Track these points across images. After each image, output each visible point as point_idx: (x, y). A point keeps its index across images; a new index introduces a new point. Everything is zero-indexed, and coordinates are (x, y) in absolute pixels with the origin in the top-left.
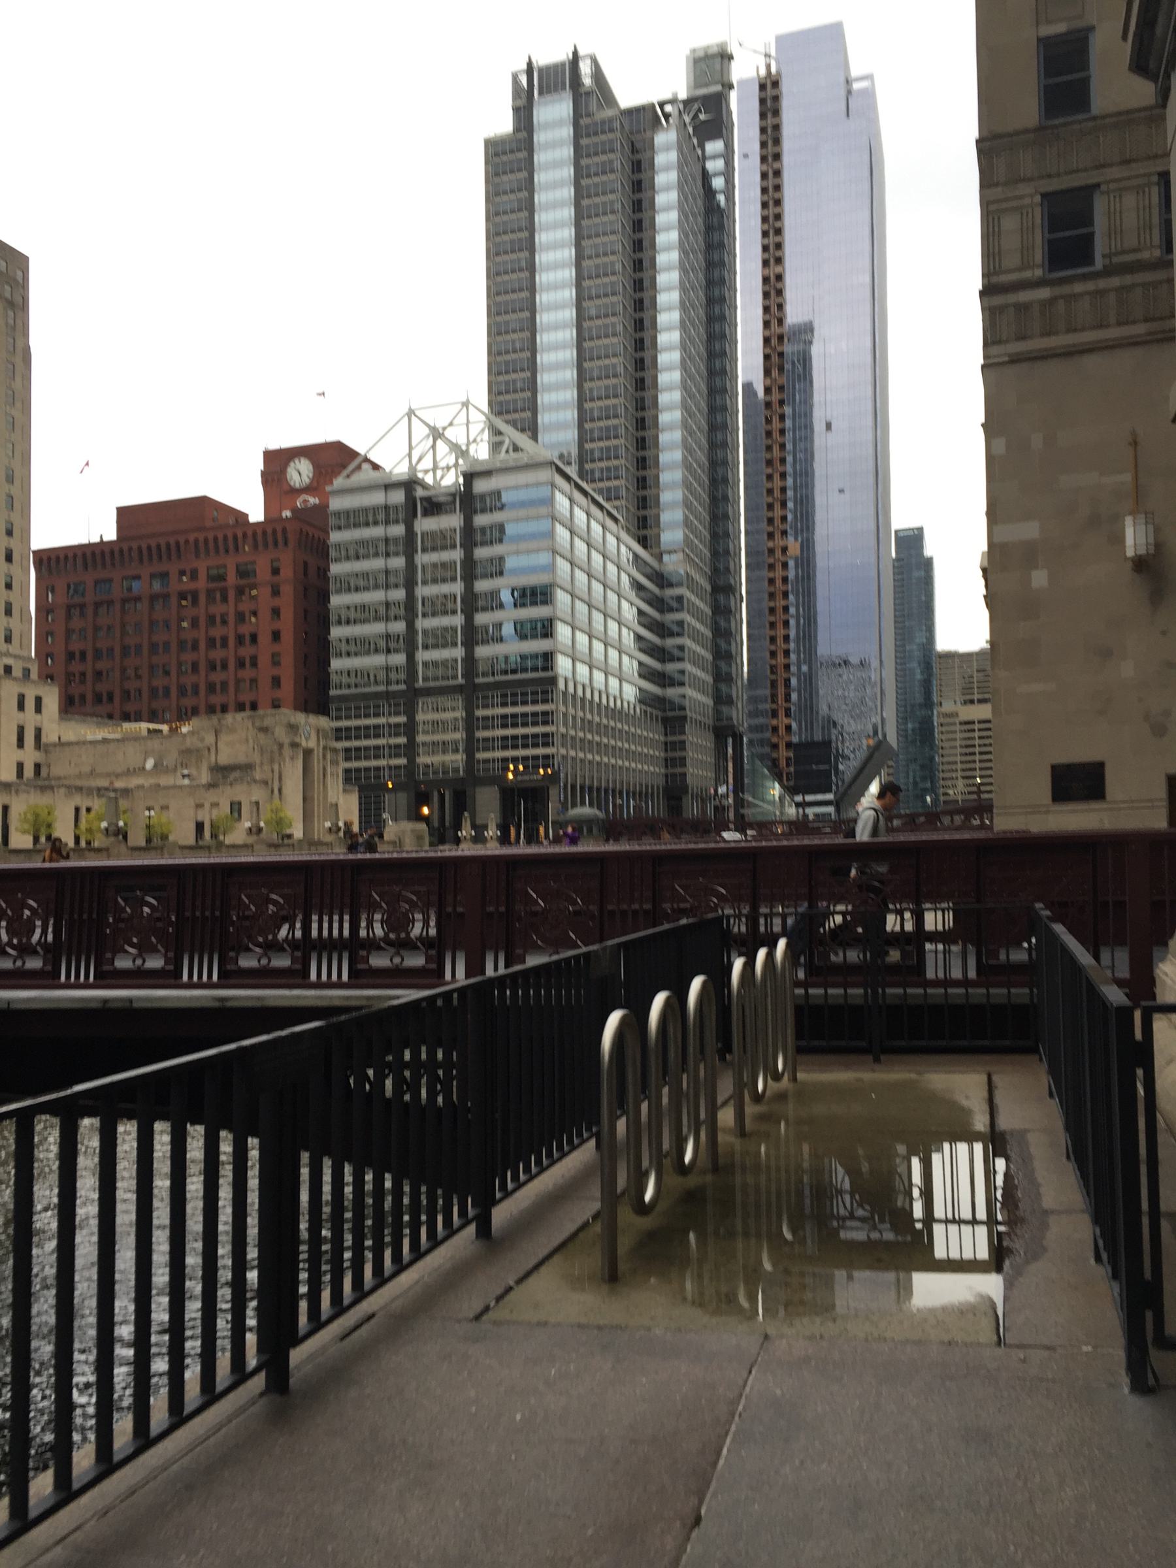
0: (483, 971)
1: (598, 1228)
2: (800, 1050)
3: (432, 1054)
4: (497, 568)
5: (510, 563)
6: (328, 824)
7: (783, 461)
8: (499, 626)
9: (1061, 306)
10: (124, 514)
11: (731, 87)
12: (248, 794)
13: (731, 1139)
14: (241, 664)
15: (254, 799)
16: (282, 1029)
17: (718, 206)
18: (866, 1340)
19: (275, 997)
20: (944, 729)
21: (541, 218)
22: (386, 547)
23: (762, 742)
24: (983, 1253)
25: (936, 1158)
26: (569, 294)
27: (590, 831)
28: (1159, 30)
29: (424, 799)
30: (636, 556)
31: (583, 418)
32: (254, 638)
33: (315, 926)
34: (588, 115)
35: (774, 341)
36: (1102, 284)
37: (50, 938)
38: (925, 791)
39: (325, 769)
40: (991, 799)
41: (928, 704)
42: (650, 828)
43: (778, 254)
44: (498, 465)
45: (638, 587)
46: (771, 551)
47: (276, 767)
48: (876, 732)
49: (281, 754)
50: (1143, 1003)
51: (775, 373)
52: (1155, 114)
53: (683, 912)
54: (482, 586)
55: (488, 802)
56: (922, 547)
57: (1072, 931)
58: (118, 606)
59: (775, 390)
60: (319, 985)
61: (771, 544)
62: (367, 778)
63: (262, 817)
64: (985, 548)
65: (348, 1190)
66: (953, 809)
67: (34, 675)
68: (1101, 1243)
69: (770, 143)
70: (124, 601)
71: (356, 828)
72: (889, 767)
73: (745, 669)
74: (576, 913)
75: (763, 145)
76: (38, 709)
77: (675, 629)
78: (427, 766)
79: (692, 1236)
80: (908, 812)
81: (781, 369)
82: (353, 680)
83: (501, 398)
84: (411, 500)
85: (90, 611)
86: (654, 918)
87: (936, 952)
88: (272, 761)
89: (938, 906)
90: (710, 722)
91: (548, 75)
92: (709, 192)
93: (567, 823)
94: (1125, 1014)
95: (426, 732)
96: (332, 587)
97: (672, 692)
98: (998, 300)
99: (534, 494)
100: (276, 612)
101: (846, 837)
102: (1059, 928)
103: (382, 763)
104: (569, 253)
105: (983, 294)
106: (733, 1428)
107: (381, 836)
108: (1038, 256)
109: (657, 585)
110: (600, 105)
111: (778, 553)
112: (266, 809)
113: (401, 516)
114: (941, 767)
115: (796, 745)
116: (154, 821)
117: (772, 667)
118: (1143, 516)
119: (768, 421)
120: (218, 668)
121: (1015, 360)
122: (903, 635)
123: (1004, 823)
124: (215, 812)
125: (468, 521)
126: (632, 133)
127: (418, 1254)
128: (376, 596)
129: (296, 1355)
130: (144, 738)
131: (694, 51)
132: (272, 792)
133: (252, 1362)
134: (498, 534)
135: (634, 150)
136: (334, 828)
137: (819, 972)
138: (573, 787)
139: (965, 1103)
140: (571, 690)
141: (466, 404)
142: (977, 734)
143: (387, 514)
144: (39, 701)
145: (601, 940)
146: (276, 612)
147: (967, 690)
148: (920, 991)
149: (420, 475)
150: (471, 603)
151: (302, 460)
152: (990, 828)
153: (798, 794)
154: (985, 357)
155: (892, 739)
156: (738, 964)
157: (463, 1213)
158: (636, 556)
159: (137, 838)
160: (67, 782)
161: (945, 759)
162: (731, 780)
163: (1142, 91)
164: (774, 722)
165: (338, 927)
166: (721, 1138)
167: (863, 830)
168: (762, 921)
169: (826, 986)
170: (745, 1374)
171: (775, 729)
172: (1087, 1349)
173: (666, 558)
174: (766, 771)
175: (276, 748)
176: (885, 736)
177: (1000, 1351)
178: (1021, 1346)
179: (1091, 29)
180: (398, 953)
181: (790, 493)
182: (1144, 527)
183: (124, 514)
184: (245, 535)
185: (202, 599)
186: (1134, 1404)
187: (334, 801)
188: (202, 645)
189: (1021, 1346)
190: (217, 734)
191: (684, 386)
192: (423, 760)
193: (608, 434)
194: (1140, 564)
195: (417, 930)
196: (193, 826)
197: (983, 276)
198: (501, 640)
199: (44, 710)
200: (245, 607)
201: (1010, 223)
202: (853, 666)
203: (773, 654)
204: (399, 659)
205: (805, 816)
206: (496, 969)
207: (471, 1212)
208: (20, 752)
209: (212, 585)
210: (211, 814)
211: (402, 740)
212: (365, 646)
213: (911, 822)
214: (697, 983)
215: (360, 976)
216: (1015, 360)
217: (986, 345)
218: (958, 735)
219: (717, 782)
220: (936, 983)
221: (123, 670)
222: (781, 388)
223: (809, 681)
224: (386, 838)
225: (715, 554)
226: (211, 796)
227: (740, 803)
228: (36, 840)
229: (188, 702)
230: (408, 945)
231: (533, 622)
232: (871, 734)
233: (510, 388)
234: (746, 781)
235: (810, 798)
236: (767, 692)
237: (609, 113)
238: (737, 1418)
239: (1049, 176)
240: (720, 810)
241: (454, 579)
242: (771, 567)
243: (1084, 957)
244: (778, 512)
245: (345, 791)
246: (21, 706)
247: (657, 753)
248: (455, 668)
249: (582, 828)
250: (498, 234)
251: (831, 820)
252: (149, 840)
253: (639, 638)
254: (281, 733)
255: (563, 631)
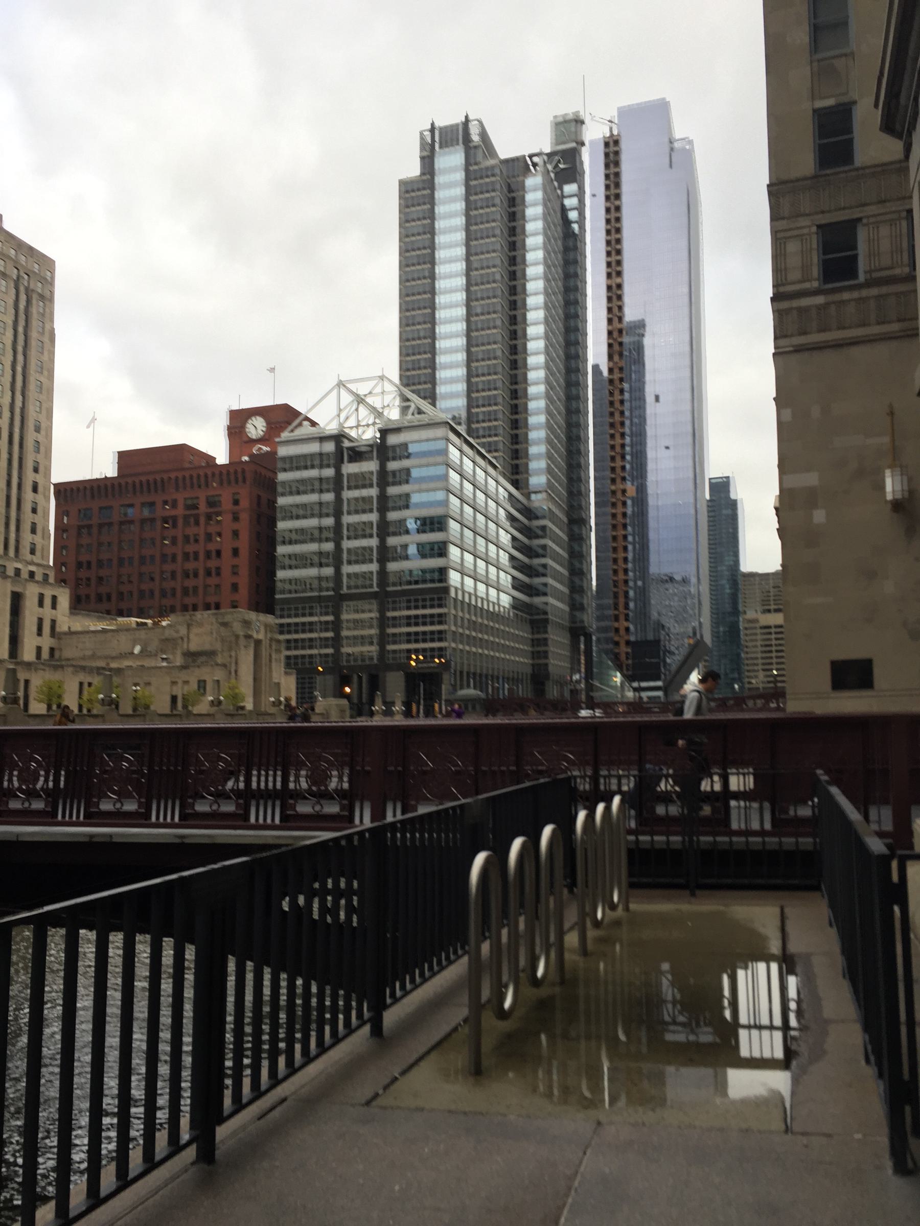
0: (384, 816)
1: (465, 1031)
2: (632, 886)
3: (349, 884)
4: (405, 502)
5: (415, 498)
6: (272, 699)
7: (622, 424)
8: (405, 547)
9: (833, 309)
10: (124, 457)
11: (583, 144)
12: (211, 675)
13: (576, 958)
14: (208, 573)
15: (216, 678)
16: (215, 863)
17: (573, 232)
18: (679, 1127)
19: (222, 836)
20: (748, 632)
21: (440, 239)
22: (320, 485)
23: (608, 641)
24: (779, 1054)
25: (741, 973)
26: (461, 296)
27: (474, 708)
28: (903, 100)
29: (346, 681)
30: (510, 495)
31: (471, 389)
32: (219, 553)
33: (254, 779)
34: (476, 164)
35: (615, 334)
36: (865, 293)
37: (51, 784)
38: (734, 680)
39: (270, 656)
40: (784, 687)
41: (736, 612)
42: (521, 706)
43: (618, 269)
44: (407, 424)
45: (511, 518)
46: (614, 493)
47: (233, 654)
48: (695, 633)
49: (237, 644)
50: (899, 852)
51: (616, 358)
52: (901, 167)
53: (541, 773)
54: (392, 516)
55: (395, 683)
56: (729, 491)
57: (845, 793)
58: (116, 528)
59: (616, 371)
60: (257, 827)
61: (613, 488)
62: (303, 663)
63: (222, 693)
64: (778, 493)
65: (284, 991)
66: (757, 695)
67: (51, 580)
68: (869, 1048)
69: (612, 186)
70: (121, 523)
71: (293, 703)
72: (706, 661)
73: (594, 583)
74: (458, 773)
75: (607, 187)
76: (54, 606)
77: (540, 551)
78: (349, 655)
79: (543, 1037)
80: (721, 696)
81: (621, 355)
82: (293, 587)
83: (408, 373)
84: (339, 450)
85: (95, 530)
86: (517, 777)
87: (739, 807)
88: (230, 649)
89: (741, 771)
90: (567, 624)
91: (446, 133)
92: (567, 222)
93: (456, 700)
94: (884, 861)
95: (348, 629)
96: (279, 515)
97: (537, 600)
98: (785, 305)
99: (432, 446)
100: (236, 534)
101: (675, 715)
102: (834, 790)
103: (314, 652)
104: (461, 266)
105: (773, 300)
106: (570, 1200)
107: (313, 709)
108: (815, 271)
109: (526, 517)
110: (485, 156)
111: (619, 495)
112: (225, 686)
113: (332, 462)
114: (746, 662)
115: (634, 643)
116: (139, 694)
117: (615, 581)
118: (899, 469)
119: (611, 394)
120: (191, 576)
121: (798, 350)
122: (715, 558)
123: (795, 706)
124: (186, 688)
125: (383, 466)
126: (508, 177)
127: (323, 1049)
128: (312, 523)
129: (222, 1132)
130: (134, 629)
131: (555, 117)
132: (230, 673)
133: (185, 1137)
134: (405, 476)
135: (510, 190)
136: (277, 703)
137: (648, 822)
138: (461, 673)
139: (762, 930)
140: (460, 597)
141: (382, 378)
142: (773, 636)
143: (321, 460)
144: (54, 598)
145: (477, 794)
146: (236, 534)
147: (765, 602)
148: (726, 839)
149: (347, 431)
150: (385, 529)
151: (258, 418)
152: (784, 710)
153: (634, 681)
154: (775, 348)
155: (708, 639)
156: (582, 815)
157: (360, 1015)
158: (510, 495)
159: (126, 708)
160: (74, 663)
161: (749, 656)
162: (583, 670)
163: (892, 148)
164: (616, 625)
165: (271, 780)
166: (567, 956)
167: (689, 708)
168: (602, 781)
169: (652, 834)
170: (581, 1154)
171: (617, 630)
172: (858, 1136)
173: (533, 497)
174: (610, 663)
175: (233, 639)
176: (702, 636)
177: (789, 1136)
178: (804, 1134)
179: (855, 103)
180: (318, 803)
181: (628, 449)
182: (899, 478)
183: (124, 457)
184: (213, 475)
185: (180, 522)
186: (897, 1185)
187: (276, 681)
188: (179, 558)
189: (804, 1134)
190: (189, 626)
191: (547, 367)
192: (346, 650)
193: (490, 402)
194: (897, 506)
195: (333, 784)
196: (168, 699)
197: (774, 286)
198: (407, 558)
199: (58, 607)
200: (212, 529)
201: (793, 247)
202: (677, 582)
203: (615, 572)
204: (329, 571)
205: (641, 698)
206: (395, 816)
207: (366, 1014)
208: (39, 638)
209: (188, 512)
210: (183, 688)
211: (330, 634)
212: (302, 561)
213: (723, 704)
214: (547, 831)
215: (290, 820)
216: (798, 350)
217: (776, 338)
218: (759, 637)
219: (574, 669)
220: (739, 833)
221: (119, 576)
222: (621, 369)
223: (643, 594)
224: (317, 710)
225: (571, 494)
226: (183, 676)
227: (590, 688)
228: (49, 707)
229: (167, 602)
230: (325, 795)
231: (432, 544)
232: (691, 635)
233: (416, 366)
234: (595, 670)
235: (644, 684)
236: (611, 602)
237: (492, 162)
238: (573, 1192)
239: (823, 212)
240: (574, 692)
241: (371, 511)
242: (614, 505)
243: (853, 814)
244: (619, 463)
245: (286, 673)
246: (41, 604)
247: (526, 648)
248: (371, 580)
249: (468, 705)
250: (407, 251)
251: (661, 703)
252: (135, 709)
253: (512, 558)
254: (238, 628)
255: (454, 552)
